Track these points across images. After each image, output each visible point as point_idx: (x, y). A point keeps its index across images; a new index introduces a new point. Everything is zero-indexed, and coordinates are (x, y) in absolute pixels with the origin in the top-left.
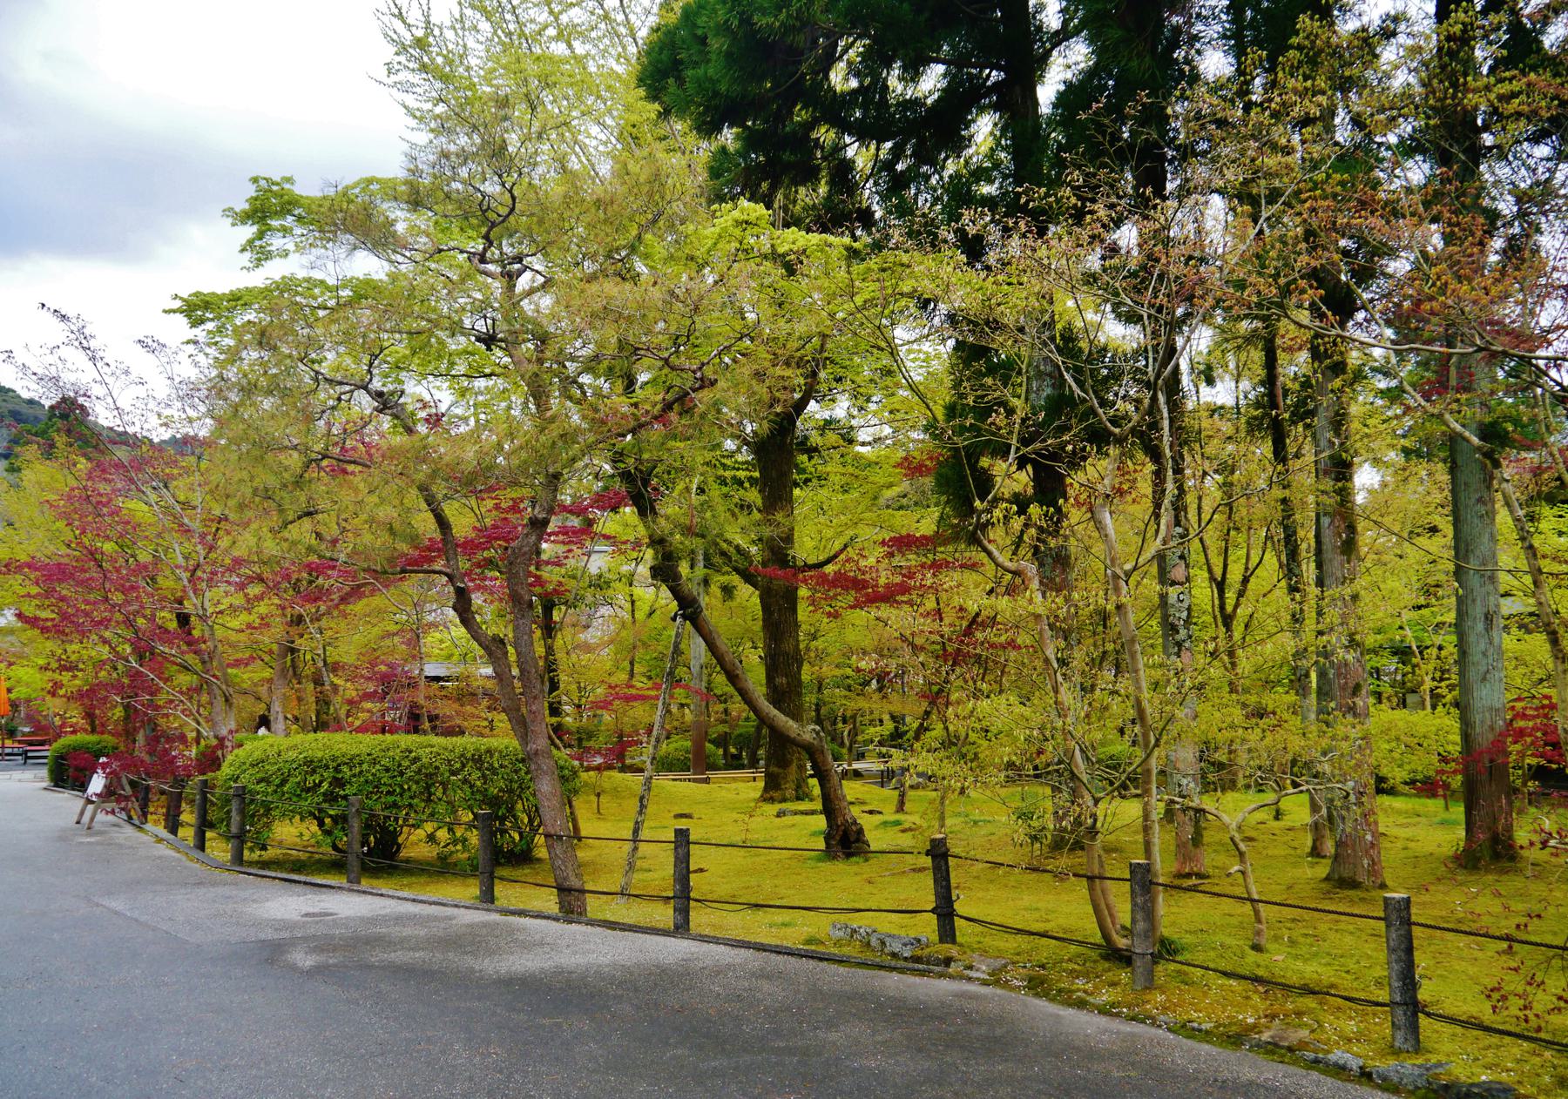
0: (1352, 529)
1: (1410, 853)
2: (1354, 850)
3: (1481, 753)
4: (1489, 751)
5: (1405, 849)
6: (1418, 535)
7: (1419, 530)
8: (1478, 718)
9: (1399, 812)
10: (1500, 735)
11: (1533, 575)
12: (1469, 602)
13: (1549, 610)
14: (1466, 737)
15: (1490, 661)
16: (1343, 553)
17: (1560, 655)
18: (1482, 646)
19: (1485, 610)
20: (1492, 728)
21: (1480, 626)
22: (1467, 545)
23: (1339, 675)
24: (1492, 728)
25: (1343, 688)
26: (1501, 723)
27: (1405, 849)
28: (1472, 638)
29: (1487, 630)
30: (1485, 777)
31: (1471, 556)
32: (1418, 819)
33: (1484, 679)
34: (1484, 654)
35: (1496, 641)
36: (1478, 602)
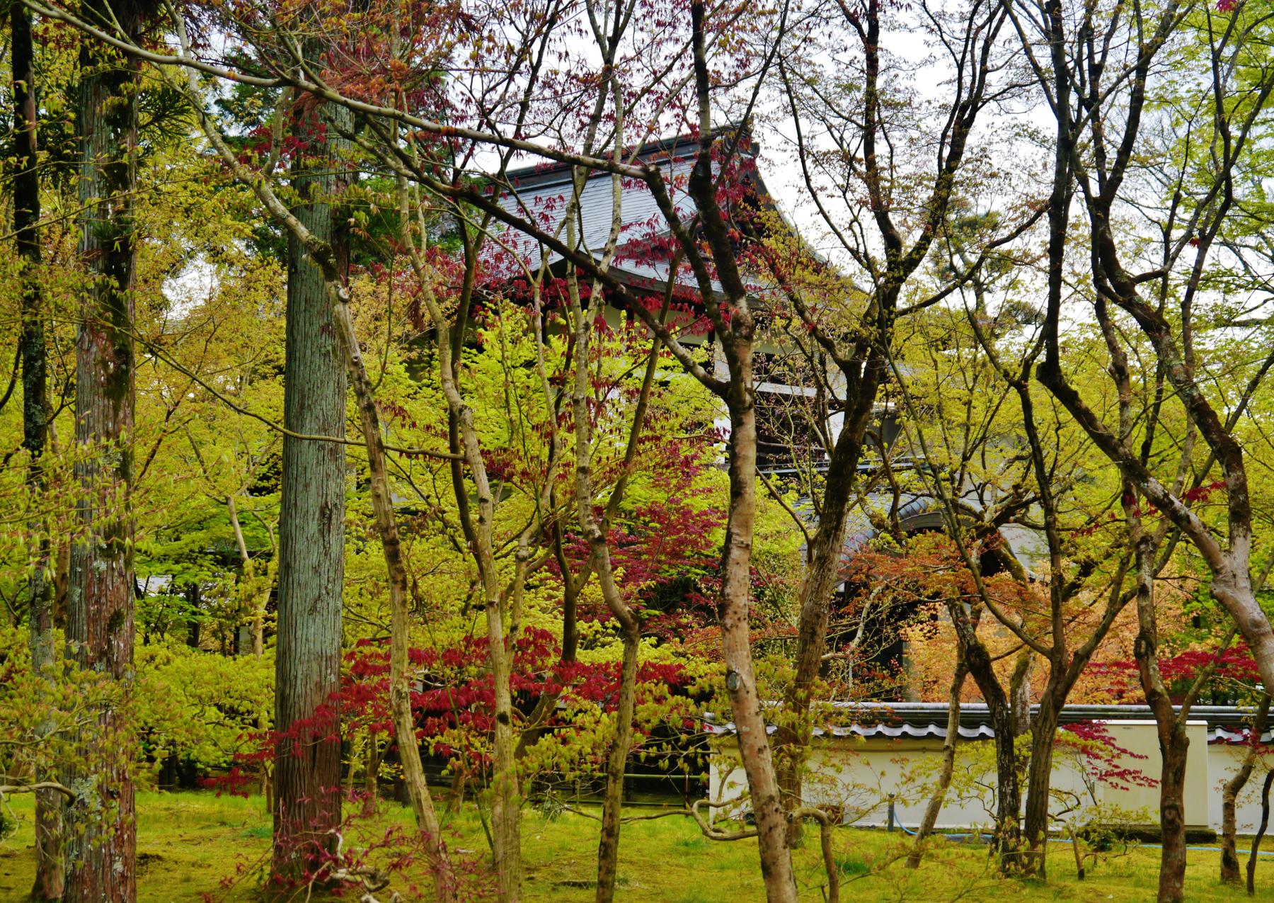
0: (124, 355)
1: (192, 888)
2: (94, 889)
3: (302, 725)
4: (312, 722)
5: (187, 880)
6: (264, 377)
7: (267, 369)
8: (300, 670)
9: (198, 818)
10: (331, 696)
11: (370, 452)
12: (300, 488)
13: (388, 507)
14: (283, 701)
15: (324, 582)
16: (108, 394)
17: (400, 578)
18: (314, 559)
19: (321, 501)
20: (320, 687)
21: (313, 527)
22: (303, 397)
23: (88, 597)
24: (320, 687)
25: (93, 620)
26: (333, 678)
27: (187, 880)
28: (300, 545)
29: (322, 532)
30: (305, 763)
31: (308, 415)
32: (219, 830)
33: (313, 610)
34: (316, 570)
35: (335, 550)
36: (313, 489)
